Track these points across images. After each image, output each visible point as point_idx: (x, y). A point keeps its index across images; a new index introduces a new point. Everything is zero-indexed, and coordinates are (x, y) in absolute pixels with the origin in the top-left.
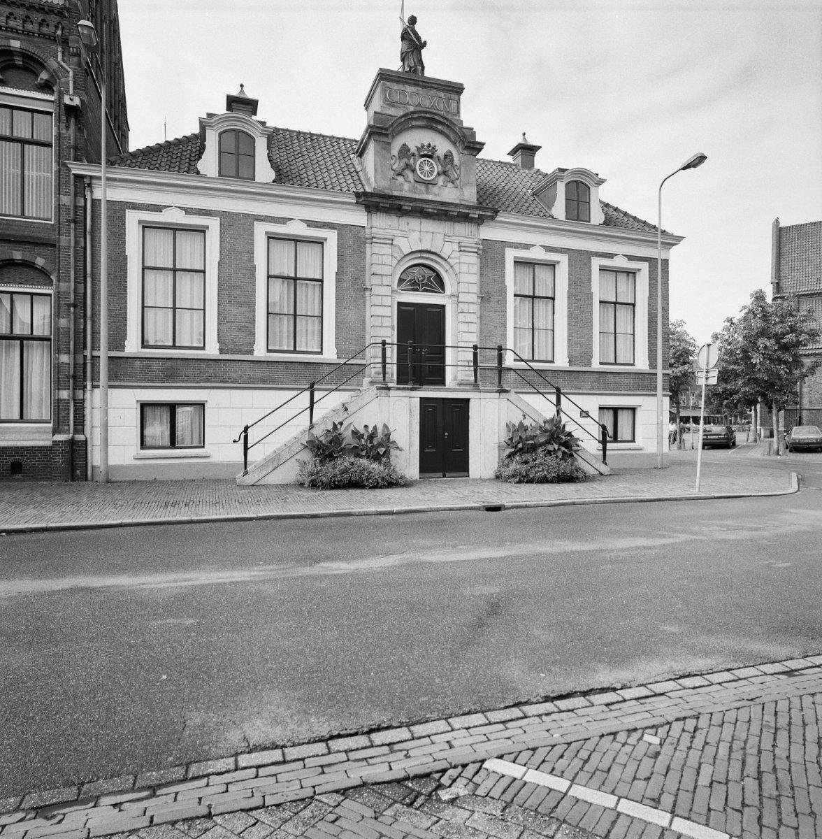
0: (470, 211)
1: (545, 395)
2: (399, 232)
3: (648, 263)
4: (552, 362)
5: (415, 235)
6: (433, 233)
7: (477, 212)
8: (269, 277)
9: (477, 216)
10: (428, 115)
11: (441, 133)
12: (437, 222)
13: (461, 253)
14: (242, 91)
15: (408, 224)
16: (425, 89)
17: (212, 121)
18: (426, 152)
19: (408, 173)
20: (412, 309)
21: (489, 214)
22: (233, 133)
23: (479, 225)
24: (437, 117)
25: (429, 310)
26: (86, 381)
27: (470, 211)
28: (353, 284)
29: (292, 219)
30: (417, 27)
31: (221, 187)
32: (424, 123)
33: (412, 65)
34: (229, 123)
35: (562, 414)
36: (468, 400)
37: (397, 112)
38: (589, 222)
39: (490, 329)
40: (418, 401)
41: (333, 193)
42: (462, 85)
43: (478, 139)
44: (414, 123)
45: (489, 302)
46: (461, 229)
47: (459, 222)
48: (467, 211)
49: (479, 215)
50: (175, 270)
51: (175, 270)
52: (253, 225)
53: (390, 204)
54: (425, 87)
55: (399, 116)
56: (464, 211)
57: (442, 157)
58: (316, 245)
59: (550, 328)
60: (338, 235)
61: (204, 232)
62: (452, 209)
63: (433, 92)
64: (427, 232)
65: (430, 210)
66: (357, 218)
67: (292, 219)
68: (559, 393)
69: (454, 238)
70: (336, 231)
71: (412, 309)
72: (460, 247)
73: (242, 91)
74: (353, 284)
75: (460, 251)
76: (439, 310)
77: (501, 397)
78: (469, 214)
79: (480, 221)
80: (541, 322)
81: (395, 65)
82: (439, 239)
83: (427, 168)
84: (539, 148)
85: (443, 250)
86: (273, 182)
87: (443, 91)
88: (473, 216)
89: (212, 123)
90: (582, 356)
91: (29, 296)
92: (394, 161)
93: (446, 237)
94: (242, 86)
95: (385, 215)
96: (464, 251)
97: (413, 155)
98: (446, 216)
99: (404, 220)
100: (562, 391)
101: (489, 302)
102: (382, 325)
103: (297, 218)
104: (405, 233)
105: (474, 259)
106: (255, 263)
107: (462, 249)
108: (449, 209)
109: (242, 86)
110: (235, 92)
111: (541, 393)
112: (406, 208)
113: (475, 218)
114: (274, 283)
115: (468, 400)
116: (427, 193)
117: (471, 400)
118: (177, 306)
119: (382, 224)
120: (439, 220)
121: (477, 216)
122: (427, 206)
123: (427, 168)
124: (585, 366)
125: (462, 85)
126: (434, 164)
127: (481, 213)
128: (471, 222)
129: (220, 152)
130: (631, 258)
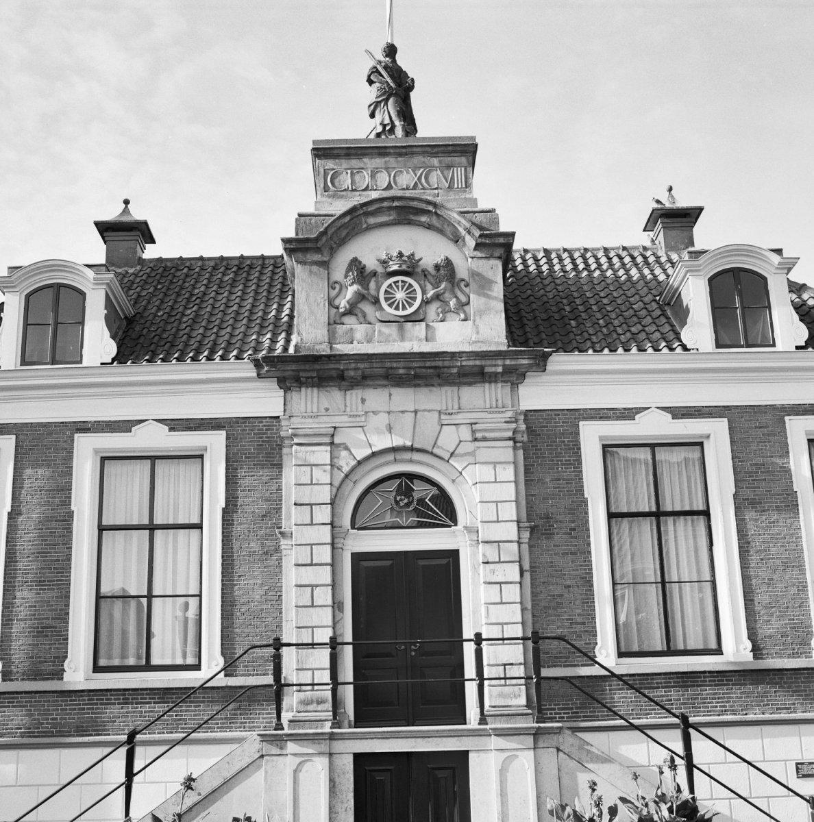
0: (483, 363)
1: (649, 732)
2: (345, 418)
3: (224, 433)
4: (718, 651)
5: (376, 425)
6: (416, 412)
7: (500, 362)
8: (102, 529)
9: (500, 369)
10: (396, 204)
11: (429, 227)
12: (425, 390)
13: (477, 444)
14: (126, 211)
15: (363, 401)
16: (400, 159)
17: (701, 262)
18: (395, 268)
19: (367, 308)
20: (388, 563)
21: (525, 362)
22: (731, 273)
23: (515, 386)
24: (415, 204)
25: (422, 563)
26: (486, 729)
27: (483, 363)
28: (250, 535)
29: (141, 421)
30: (401, 60)
31: (61, 381)
32: (392, 218)
33: (387, 121)
34: (729, 259)
35: (168, 797)
36: (465, 754)
37: (339, 207)
38: (774, 345)
39: (556, 592)
40: (349, 760)
41: (697, 357)
42: (473, 138)
43: (504, 228)
44: (372, 220)
45: (549, 536)
46: (475, 397)
47: (470, 384)
48: (478, 363)
49: (504, 366)
50: (152, 528)
51: (152, 528)
52: (73, 441)
53: (318, 371)
54: (400, 155)
55: (339, 213)
56: (471, 363)
57: (431, 270)
58: (642, 449)
59: (707, 577)
60: (228, 438)
61: (201, 457)
62: (447, 364)
63: (417, 160)
64: (403, 412)
65: (401, 371)
66: (263, 400)
67: (141, 421)
68: (686, 726)
69: (460, 416)
70: (224, 433)
71: (388, 563)
72: (473, 432)
73: (126, 211)
74: (250, 535)
75: (476, 440)
76: (444, 561)
77: (541, 744)
78: (482, 367)
79: (513, 377)
80: (682, 565)
81: (359, 126)
82: (429, 423)
83: (400, 295)
84: (97, 224)
85: (439, 443)
86: (113, 360)
87: (434, 155)
88: (493, 369)
89: (700, 266)
90: (784, 635)
91: (198, 593)
92: (337, 290)
93: (443, 417)
94: (127, 202)
95: (315, 390)
96: (485, 439)
97: (374, 274)
98: (439, 376)
99: (354, 396)
100: (691, 720)
101: (549, 536)
102: (311, 609)
103: (654, 405)
104: (358, 419)
105: (505, 452)
106: (73, 508)
107: (479, 435)
108: (440, 364)
109: (127, 202)
110: (111, 213)
111: (641, 729)
112: (352, 373)
113: (496, 374)
114: (640, 526)
115: (465, 754)
116: (402, 338)
117: (471, 755)
118: (155, 593)
119: (312, 408)
120: (426, 385)
121: (500, 369)
122: (395, 365)
123: (400, 295)
124: (794, 655)
125: (473, 138)
126: (416, 286)
127: (508, 362)
128: (496, 382)
129: (26, 325)
130: (176, 425)
